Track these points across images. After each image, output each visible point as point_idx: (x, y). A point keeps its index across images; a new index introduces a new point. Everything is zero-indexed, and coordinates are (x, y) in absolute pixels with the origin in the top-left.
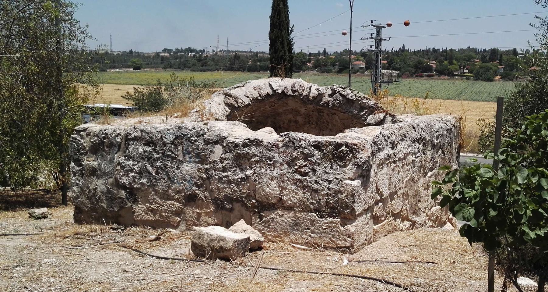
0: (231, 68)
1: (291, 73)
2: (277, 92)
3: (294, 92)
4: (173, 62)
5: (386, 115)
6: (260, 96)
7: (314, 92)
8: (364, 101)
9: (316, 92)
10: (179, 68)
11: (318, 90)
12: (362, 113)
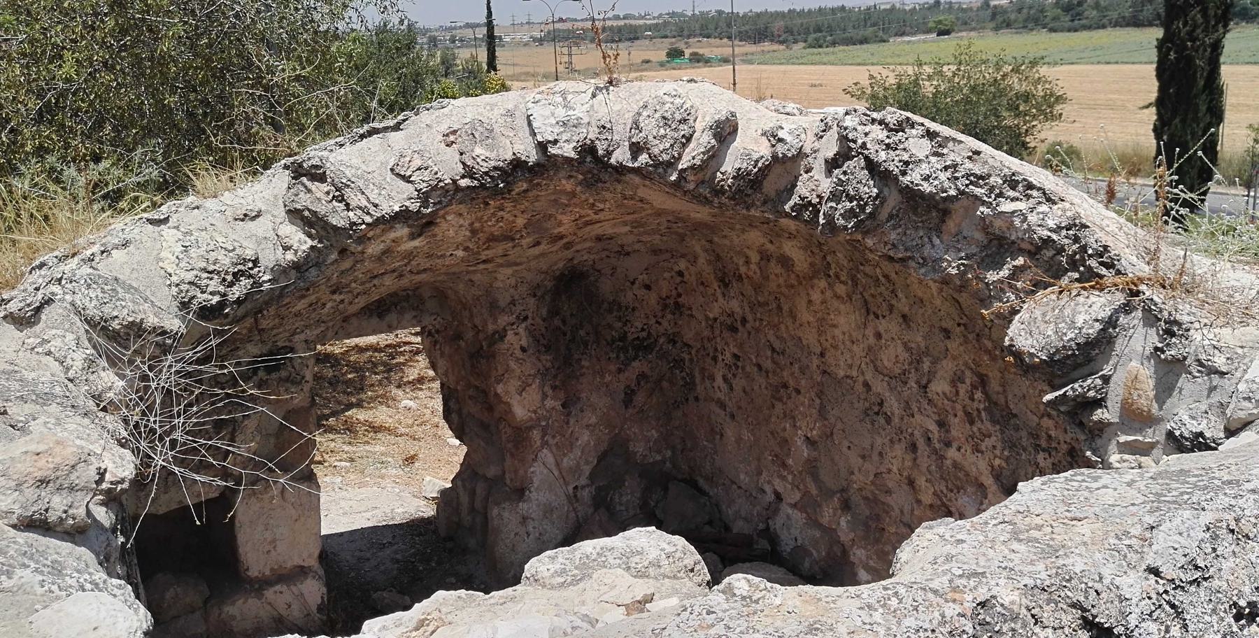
0: (745, 37)
1: (1225, 26)
2: (553, 150)
3: (636, 149)
4: (1013, 17)
5: (1127, 308)
6: (469, 173)
7: (749, 148)
8: (1007, 207)
9: (763, 150)
10: (1025, 27)
11: (774, 137)
12: (992, 276)
